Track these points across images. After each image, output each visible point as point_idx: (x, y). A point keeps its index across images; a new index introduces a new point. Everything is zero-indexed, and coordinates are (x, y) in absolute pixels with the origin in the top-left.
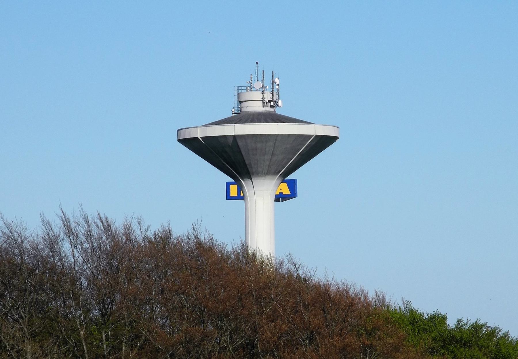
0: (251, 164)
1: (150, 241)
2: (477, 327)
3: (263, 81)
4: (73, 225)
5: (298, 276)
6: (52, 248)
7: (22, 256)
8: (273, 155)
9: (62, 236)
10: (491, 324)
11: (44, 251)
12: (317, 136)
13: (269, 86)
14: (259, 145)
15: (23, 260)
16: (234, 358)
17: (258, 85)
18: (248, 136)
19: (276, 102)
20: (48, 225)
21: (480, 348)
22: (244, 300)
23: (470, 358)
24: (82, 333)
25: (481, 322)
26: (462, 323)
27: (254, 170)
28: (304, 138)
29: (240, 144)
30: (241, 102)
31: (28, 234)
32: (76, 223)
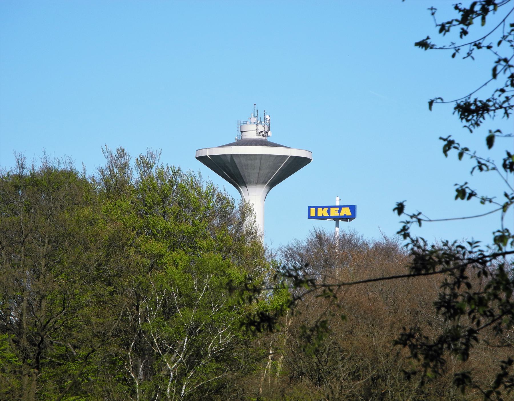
0: (245, 176)
8: (260, 169)
12: (291, 156)
14: (249, 162)
16: (389, 400)
18: (241, 155)
19: (267, 132)
27: (248, 180)
29: (236, 160)
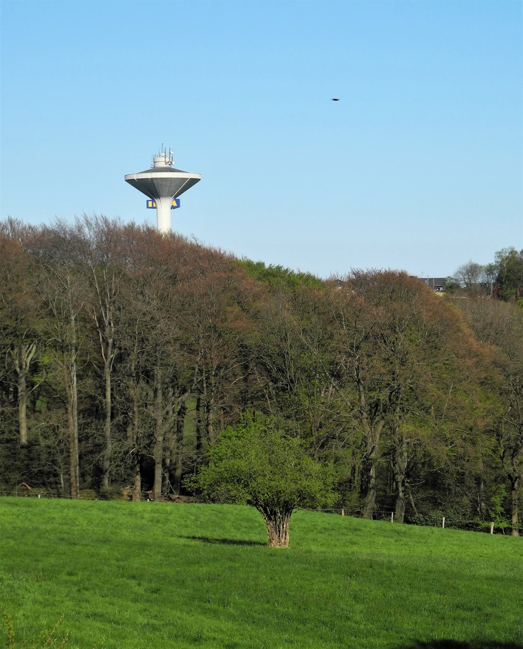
1: (126, 228)
2: (279, 268)
3: (165, 152)
4: (89, 220)
5: (197, 244)
6: (79, 231)
7: (65, 235)
8: (170, 187)
9: (85, 225)
10: (285, 267)
11: (75, 232)
13: (168, 155)
15: (66, 237)
17: (163, 154)
20: (78, 220)
21: (281, 277)
22: (171, 255)
23: (522, 287)
24: (94, 271)
25: (280, 265)
26: (272, 266)
28: (184, 179)
29: (155, 182)
30: (155, 162)
31: (68, 224)
32: (91, 219)
